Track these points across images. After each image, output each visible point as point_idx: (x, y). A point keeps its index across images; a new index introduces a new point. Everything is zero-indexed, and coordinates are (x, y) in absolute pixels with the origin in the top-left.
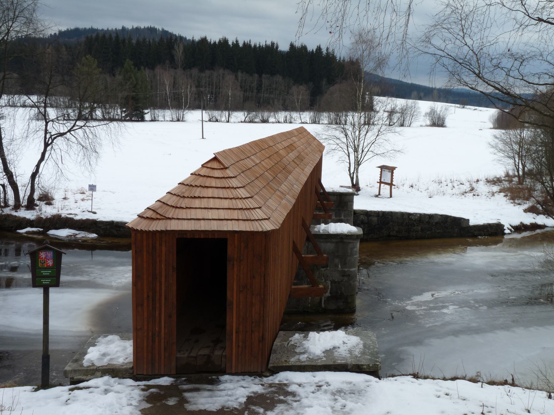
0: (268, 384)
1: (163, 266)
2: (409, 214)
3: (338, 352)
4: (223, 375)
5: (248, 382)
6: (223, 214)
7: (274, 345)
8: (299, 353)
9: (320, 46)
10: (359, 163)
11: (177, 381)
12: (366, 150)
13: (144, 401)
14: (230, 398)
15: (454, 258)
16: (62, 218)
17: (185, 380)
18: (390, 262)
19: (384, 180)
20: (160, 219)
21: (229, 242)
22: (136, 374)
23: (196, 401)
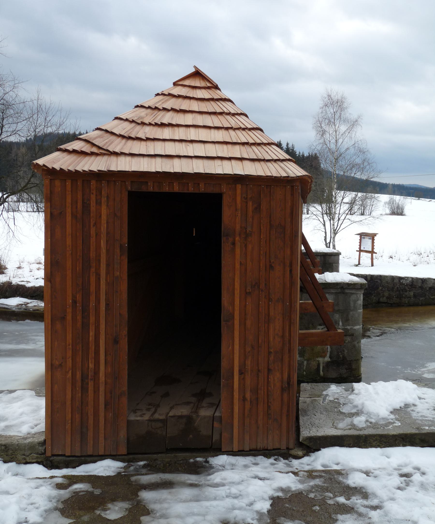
0: (304, 471)
1: (103, 244)
2: (400, 278)
3: (418, 413)
4: (217, 456)
5: (266, 468)
6: (212, 150)
7: (300, 402)
8: (349, 414)
9: (280, 142)
10: (335, 231)
11: (129, 467)
12: (343, 218)
13: (57, 511)
14: (236, 501)
15: (331, 393)
16: (13, 285)
17: (145, 465)
18: (387, 328)
19: (364, 248)
20: (97, 155)
21: (226, 201)
22: (50, 455)
23: (167, 509)
